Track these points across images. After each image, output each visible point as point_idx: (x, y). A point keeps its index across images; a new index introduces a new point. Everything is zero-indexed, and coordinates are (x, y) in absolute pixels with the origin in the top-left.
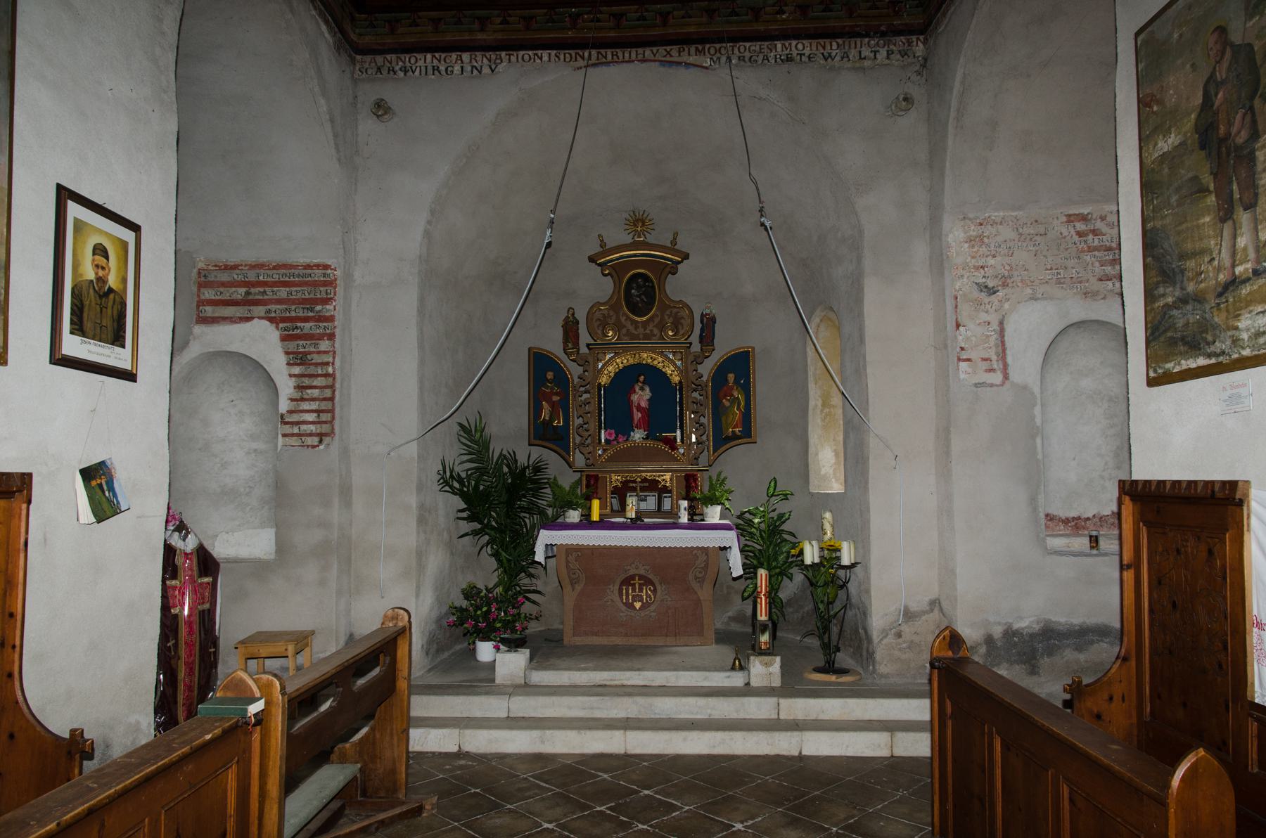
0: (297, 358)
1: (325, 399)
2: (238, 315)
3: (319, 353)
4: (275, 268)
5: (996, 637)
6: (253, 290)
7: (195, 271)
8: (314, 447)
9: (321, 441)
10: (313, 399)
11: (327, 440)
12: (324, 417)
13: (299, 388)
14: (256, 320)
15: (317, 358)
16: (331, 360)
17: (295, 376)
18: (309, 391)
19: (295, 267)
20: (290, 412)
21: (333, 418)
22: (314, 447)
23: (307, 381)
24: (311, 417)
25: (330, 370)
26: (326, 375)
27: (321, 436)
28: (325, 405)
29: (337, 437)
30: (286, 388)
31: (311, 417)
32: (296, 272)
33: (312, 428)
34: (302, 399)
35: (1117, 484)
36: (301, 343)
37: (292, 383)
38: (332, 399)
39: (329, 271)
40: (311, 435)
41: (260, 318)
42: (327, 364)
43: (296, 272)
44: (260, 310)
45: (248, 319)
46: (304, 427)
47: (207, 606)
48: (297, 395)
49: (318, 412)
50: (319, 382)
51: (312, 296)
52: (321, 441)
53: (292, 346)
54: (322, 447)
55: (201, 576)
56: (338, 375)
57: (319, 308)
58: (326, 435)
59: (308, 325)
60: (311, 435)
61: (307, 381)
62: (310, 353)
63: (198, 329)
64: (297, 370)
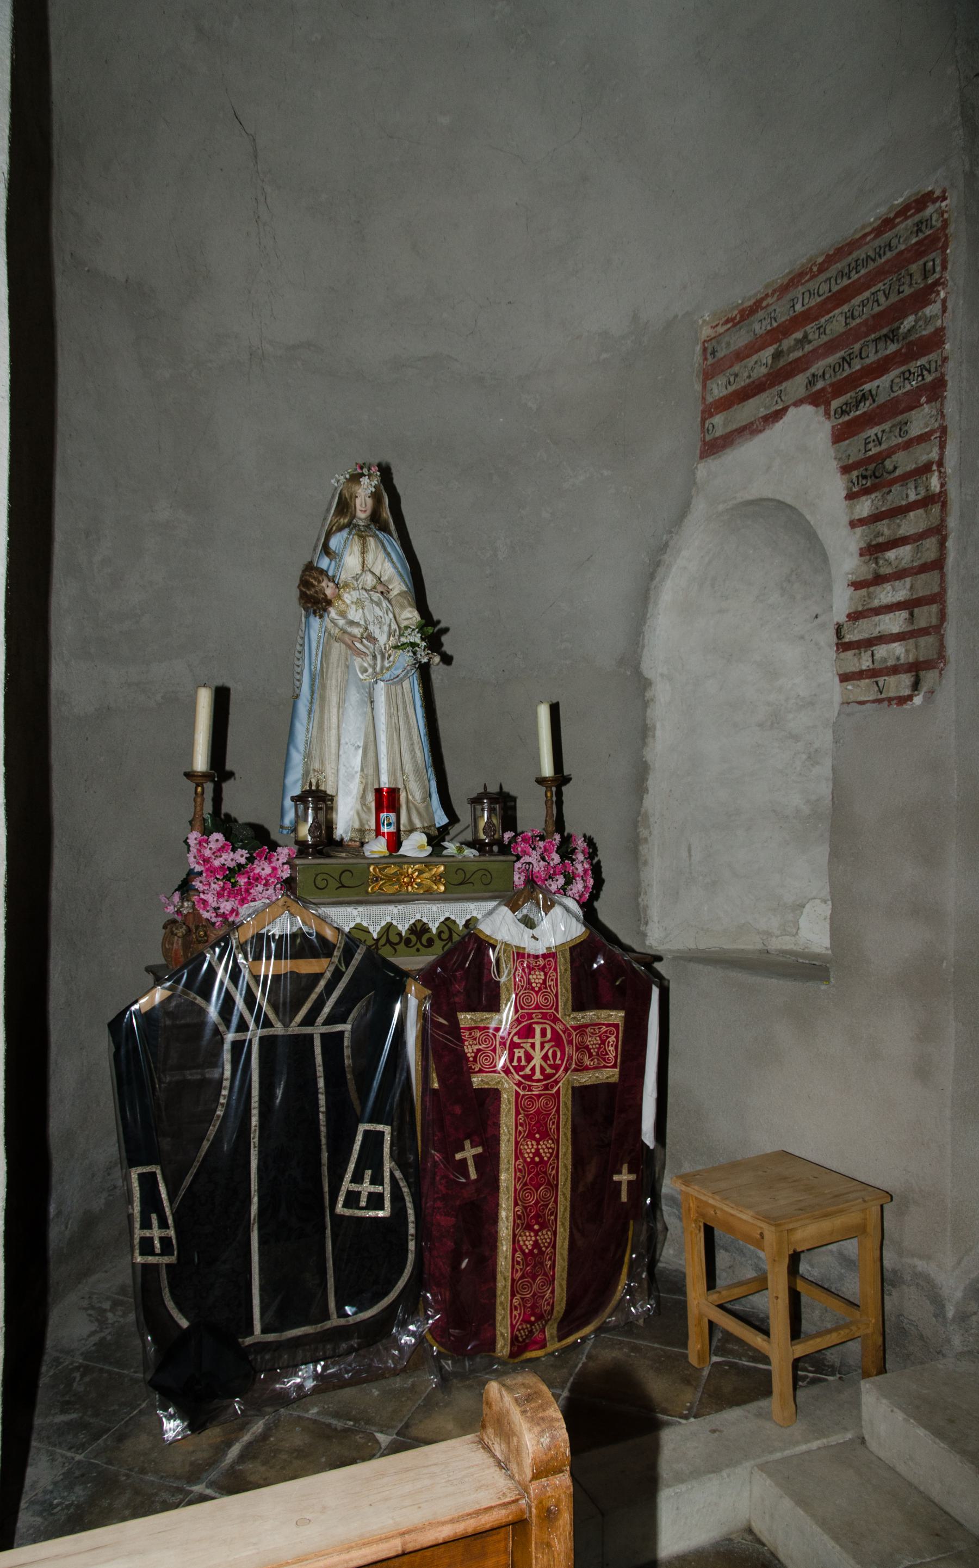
0: (867, 476)
1: (924, 568)
2: (763, 412)
3: (908, 445)
4: (822, 269)
5: (357, 488)
6: (787, 343)
7: (698, 348)
8: (902, 700)
9: (916, 686)
10: (900, 575)
11: (929, 678)
12: (926, 616)
13: (873, 550)
14: (792, 411)
15: (904, 462)
16: (934, 455)
17: (862, 522)
18: (891, 555)
19: (853, 245)
20: (855, 616)
21: (942, 616)
22: (902, 700)
23: (886, 530)
24: (894, 623)
25: (935, 483)
26: (927, 501)
27: (916, 669)
28: (925, 584)
29: (951, 669)
30: (845, 555)
31: (894, 623)
32: (860, 254)
33: (898, 649)
34: (879, 579)
35: (460, 817)
36: (872, 432)
37: (854, 541)
38: (938, 564)
39: (930, 209)
40: (895, 670)
41: (797, 404)
42: (926, 469)
43: (860, 254)
44: (797, 386)
45: (777, 415)
46: (881, 651)
47: (610, 1075)
48: (866, 572)
49: (909, 605)
50: (912, 523)
51: (894, 298)
52: (916, 686)
53: (855, 448)
54: (918, 700)
55: (579, 1005)
56: (953, 493)
57: (909, 322)
58: (928, 665)
59: (883, 382)
60: (895, 670)
61: (886, 530)
62: (890, 452)
63: (703, 470)
64: (865, 507)
